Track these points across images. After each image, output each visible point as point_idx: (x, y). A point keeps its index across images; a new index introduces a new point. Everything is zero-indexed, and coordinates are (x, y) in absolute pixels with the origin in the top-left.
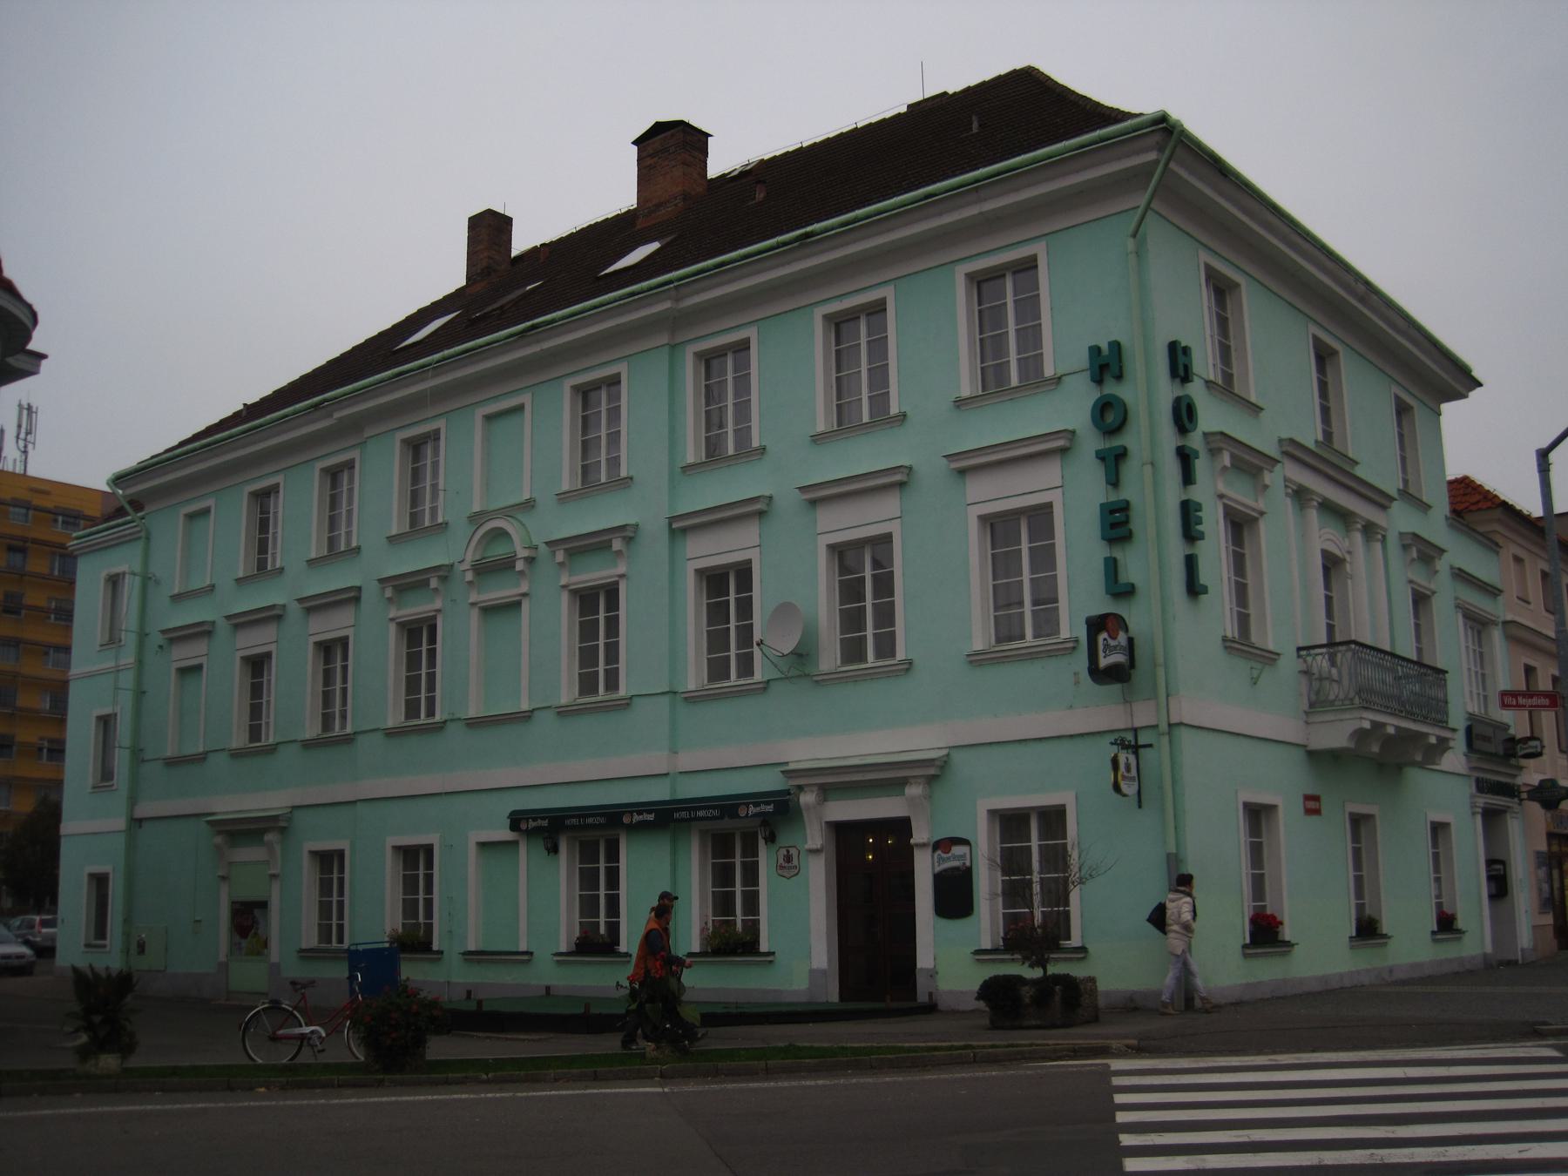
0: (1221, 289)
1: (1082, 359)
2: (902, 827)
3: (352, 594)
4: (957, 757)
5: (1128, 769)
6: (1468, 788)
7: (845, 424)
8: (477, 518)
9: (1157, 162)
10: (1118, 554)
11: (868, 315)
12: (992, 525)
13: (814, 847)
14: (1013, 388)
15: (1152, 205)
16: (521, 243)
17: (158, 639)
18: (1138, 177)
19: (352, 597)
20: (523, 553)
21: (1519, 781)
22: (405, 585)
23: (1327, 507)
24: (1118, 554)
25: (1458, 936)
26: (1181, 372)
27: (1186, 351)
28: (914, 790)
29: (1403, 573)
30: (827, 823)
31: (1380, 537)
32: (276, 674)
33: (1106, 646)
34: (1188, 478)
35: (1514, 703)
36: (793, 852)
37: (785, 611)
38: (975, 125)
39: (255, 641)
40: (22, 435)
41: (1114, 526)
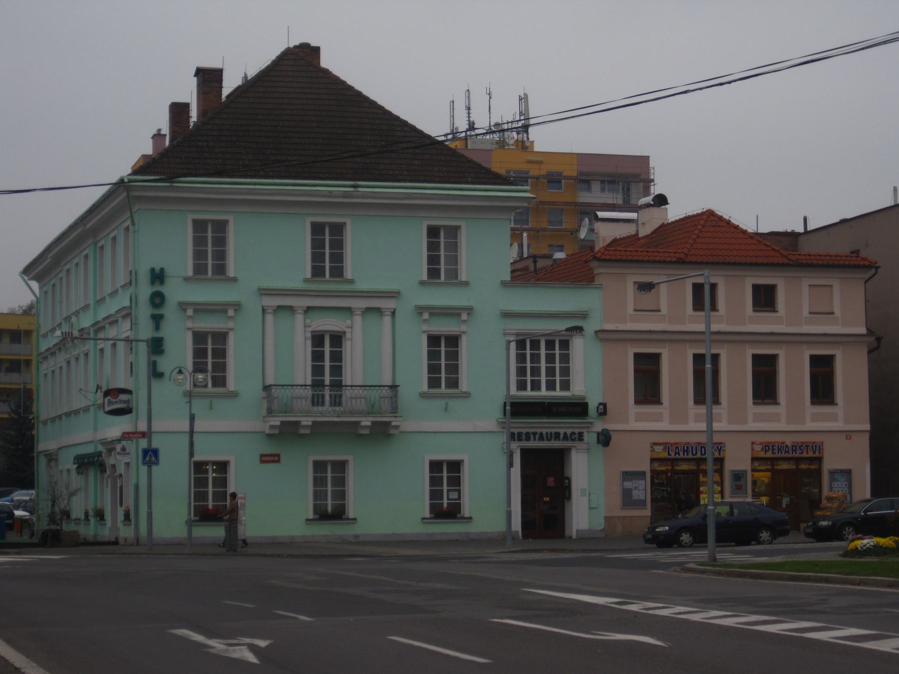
16: (230, 84)
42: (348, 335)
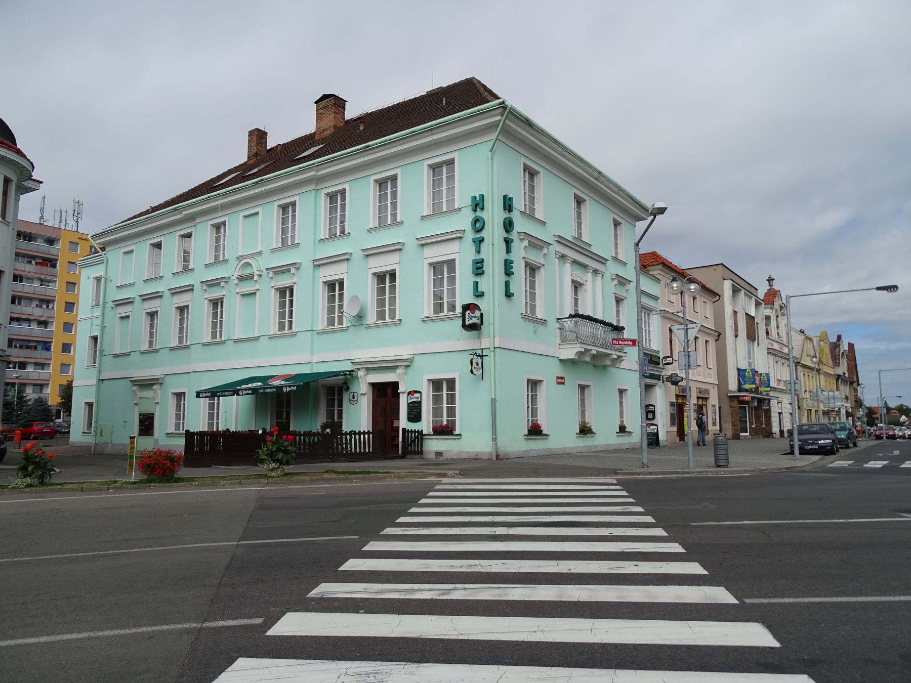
0: (531, 174)
1: (469, 202)
2: (395, 385)
4: (417, 358)
5: (477, 364)
6: (637, 376)
7: (382, 224)
8: (240, 258)
9: (500, 120)
11: (447, 165)
12: (434, 267)
13: (363, 393)
15: (498, 138)
16: (271, 144)
17: (111, 304)
18: (492, 127)
19: (190, 289)
20: (256, 273)
21: (663, 373)
22: (213, 284)
23: (575, 262)
25: (592, 435)
26: (507, 207)
27: (511, 199)
28: (399, 371)
29: (612, 288)
30: (369, 383)
31: (601, 275)
32: (160, 320)
33: (469, 316)
34: (508, 251)
35: (618, 343)
36: (355, 394)
37: (355, 298)
38: (444, 102)
41: (477, 269)
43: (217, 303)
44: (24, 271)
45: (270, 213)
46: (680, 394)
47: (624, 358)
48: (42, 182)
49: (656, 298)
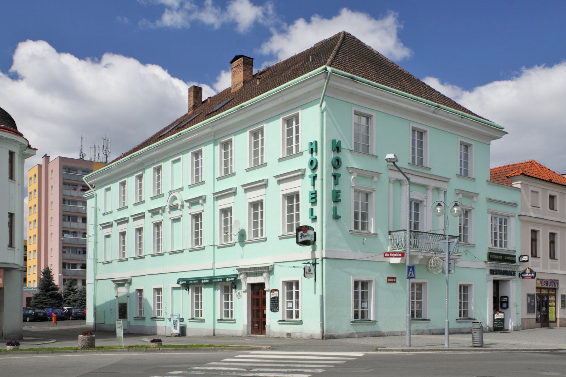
2: (262, 285)
3: (300, 173)
10: (313, 207)
14: (294, 155)
19: (264, 184)
20: (180, 204)
24: (313, 207)
28: (265, 275)
35: (389, 255)
38: (311, 60)
39: (255, 196)
40: (105, 149)
41: (312, 198)
42: (425, 203)
43: (158, 225)
44: (70, 196)
45: (187, 158)
46: (543, 287)
47: (458, 260)
48: (37, 150)
49: (514, 205)
